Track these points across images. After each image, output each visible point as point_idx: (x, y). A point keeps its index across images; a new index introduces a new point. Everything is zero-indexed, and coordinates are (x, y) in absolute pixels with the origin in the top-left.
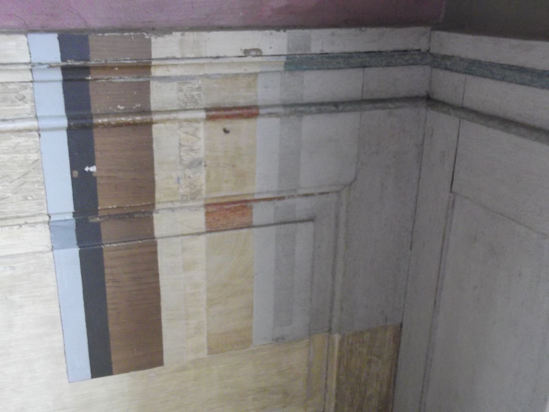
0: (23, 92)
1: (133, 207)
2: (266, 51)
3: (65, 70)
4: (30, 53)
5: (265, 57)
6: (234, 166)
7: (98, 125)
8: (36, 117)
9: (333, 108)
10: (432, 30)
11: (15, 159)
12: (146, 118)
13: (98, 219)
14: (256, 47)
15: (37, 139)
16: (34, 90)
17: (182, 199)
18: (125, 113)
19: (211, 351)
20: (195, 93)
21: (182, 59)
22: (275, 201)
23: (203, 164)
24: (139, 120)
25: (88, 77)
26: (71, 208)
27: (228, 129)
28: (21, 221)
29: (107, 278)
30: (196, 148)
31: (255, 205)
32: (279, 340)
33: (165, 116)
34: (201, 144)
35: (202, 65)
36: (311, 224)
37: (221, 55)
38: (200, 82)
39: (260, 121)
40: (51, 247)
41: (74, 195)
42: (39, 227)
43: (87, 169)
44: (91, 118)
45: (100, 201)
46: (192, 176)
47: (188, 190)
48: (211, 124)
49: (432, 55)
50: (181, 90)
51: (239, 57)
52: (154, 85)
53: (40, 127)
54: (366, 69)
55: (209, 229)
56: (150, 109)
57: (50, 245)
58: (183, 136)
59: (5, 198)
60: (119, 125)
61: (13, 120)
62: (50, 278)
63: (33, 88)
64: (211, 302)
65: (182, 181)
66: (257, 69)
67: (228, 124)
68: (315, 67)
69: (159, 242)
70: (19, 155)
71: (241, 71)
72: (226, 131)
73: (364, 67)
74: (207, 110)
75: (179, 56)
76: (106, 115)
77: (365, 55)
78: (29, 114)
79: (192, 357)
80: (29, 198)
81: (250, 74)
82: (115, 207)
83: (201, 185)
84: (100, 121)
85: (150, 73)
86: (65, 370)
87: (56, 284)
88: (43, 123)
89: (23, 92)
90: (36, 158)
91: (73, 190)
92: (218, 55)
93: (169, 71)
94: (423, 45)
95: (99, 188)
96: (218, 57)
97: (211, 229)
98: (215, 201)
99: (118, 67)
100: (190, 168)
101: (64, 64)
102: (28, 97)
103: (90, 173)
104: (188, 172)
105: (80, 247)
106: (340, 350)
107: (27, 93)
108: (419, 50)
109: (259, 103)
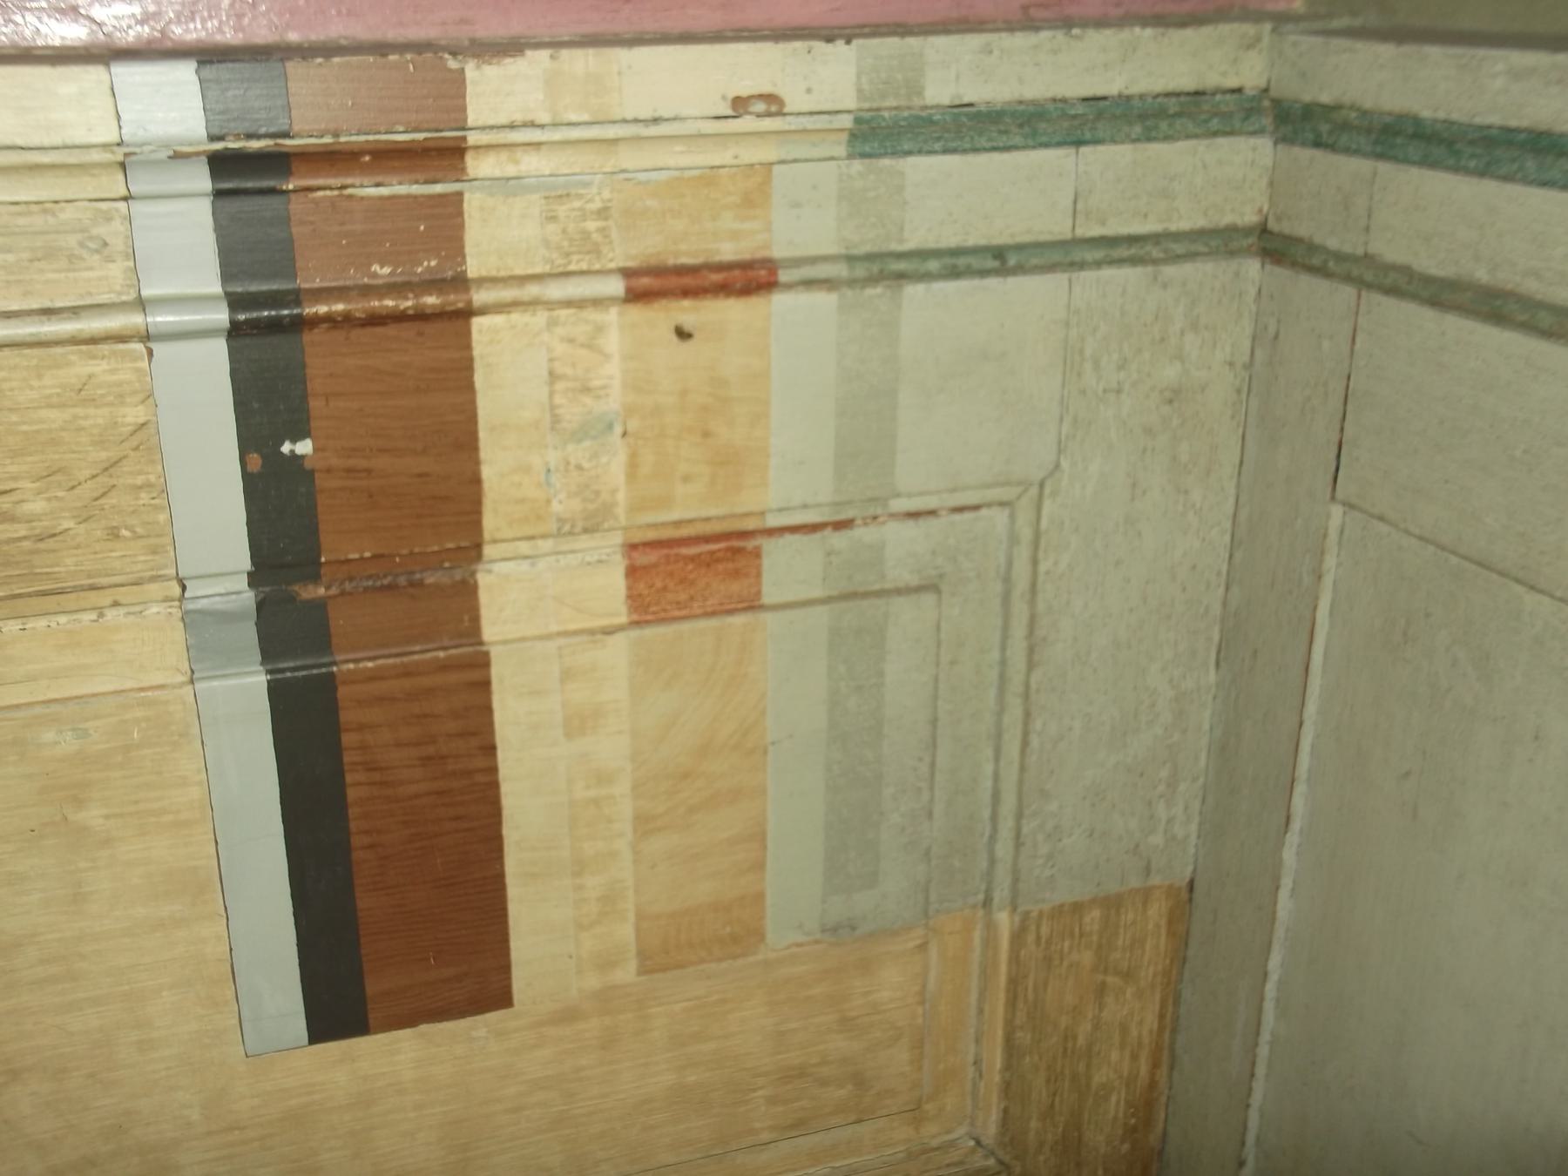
2: (795, 100)
6: (706, 434)
12: (455, 300)
14: (766, 89)
17: (559, 529)
20: (592, 225)
22: (828, 532)
23: (618, 430)
24: (433, 306)
27: (687, 328)
29: (347, 758)
30: (596, 383)
31: (769, 546)
34: (612, 371)
36: (928, 599)
40: (189, 672)
43: (286, 448)
45: (326, 540)
46: (586, 465)
50: (553, 219)
54: (1084, 150)
55: (635, 617)
58: (560, 349)
59: (54, 535)
64: (645, 825)
67: (687, 312)
68: (937, 146)
70: (92, 411)
72: (683, 334)
73: (1079, 143)
74: (627, 273)
75: (544, 117)
78: (120, 293)
79: (593, 982)
80: (125, 533)
82: (367, 554)
85: (463, 170)
89: (101, 230)
90: (141, 420)
92: (657, 115)
93: (517, 162)
96: (656, 121)
102: (118, 244)
104: (578, 452)
105: (269, 672)
109: (777, 253)
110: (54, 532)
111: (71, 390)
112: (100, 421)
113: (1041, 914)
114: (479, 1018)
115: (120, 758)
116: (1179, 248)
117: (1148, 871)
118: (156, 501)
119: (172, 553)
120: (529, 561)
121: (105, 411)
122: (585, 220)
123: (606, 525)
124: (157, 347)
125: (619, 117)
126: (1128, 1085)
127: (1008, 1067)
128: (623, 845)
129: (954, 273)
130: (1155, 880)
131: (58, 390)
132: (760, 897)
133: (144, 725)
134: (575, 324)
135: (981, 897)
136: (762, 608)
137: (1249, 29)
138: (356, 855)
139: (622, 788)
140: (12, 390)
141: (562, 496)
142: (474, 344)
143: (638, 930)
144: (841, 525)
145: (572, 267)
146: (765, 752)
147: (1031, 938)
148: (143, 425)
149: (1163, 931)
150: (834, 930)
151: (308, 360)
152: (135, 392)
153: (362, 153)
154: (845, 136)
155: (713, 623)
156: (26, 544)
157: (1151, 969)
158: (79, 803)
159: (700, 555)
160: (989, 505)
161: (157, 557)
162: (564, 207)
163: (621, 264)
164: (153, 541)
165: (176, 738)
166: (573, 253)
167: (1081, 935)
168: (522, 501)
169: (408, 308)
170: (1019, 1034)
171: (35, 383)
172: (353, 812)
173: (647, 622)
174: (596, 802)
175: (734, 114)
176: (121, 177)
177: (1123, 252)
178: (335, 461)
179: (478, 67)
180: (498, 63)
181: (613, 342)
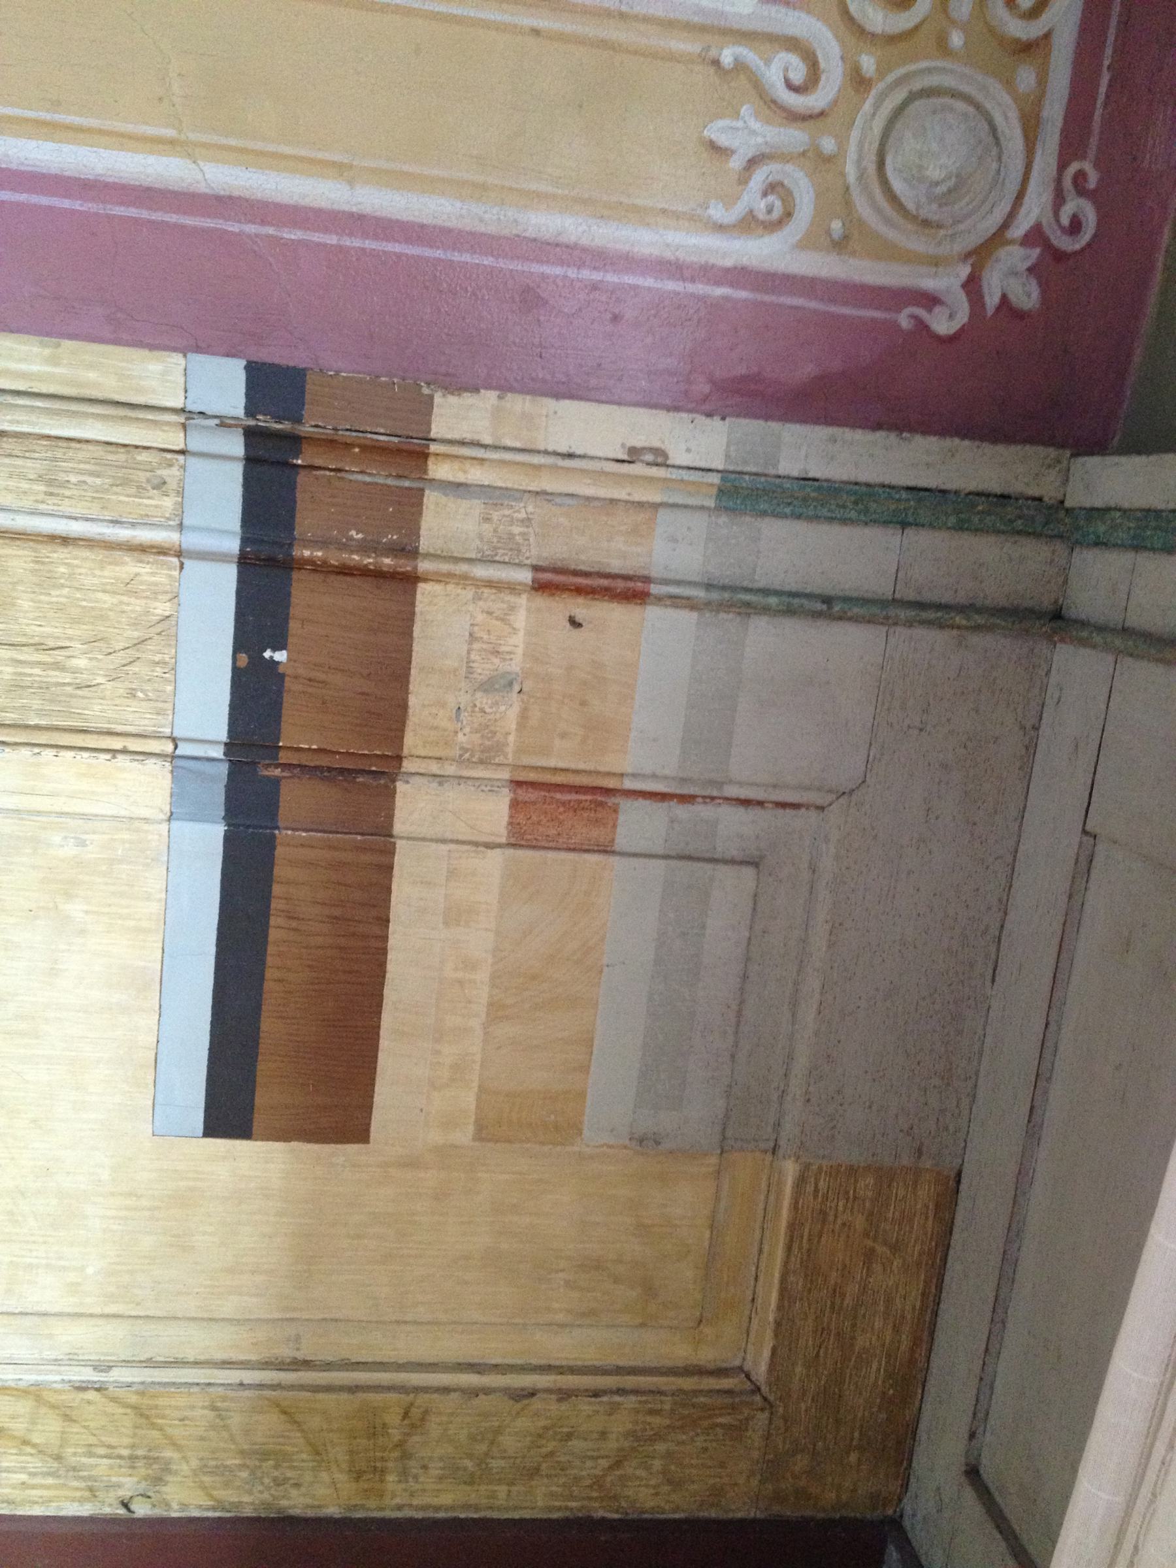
0: (164, 473)
1: (353, 753)
2: (678, 457)
3: (252, 435)
4: (186, 392)
5: (674, 471)
6: (583, 703)
7: (302, 564)
8: (181, 526)
9: (820, 606)
10: (1073, 455)
11: (125, 608)
12: (405, 566)
13: (277, 772)
14: (656, 443)
15: (176, 573)
16: (185, 471)
17: (461, 756)
18: (364, 548)
19: (482, 1133)
20: (516, 530)
21: (496, 448)
22: (674, 803)
23: (517, 688)
24: (389, 566)
25: (297, 459)
26: (219, 730)
27: (579, 619)
28: (117, 744)
29: (275, 904)
30: (503, 649)
31: (625, 804)
32: (645, 1142)
33: (445, 567)
34: (517, 642)
35: (538, 467)
36: (748, 872)
37: (579, 452)
38: (530, 509)
39: (652, 612)
40: (169, 814)
41: (233, 707)
42: (152, 764)
43: (267, 654)
44: (291, 545)
45: (286, 727)
46: (488, 710)
47: (476, 738)
48: (542, 601)
49: (1068, 511)
50: (487, 520)
51: (618, 461)
52: (431, 498)
53: (184, 546)
54: (910, 532)
55: (513, 841)
56: (417, 548)
57: (167, 809)
58: (480, 618)
59: (89, 686)
60: (345, 571)
61: (133, 525)
62: (154, 881)
63: (183, 467)
64: (497, 1012)
65: (464, 715)
66: (657, 498)
67: (581, 608)
68: (788, 510)
69: (400, 845)
70: (132, 600)
71: (621, 494)
72: (575, 623)
73: (904, 525)
74: (536, 568)
75: (487, 439)
76: (323, 544)
77: (904, 495)
78: (168, 519)
79: (436, 1137)
80: (140, 694)
81: (641, 505)
82: (314, 747)
83: (508, 734)
84: (307, 553)
85: (425, 472)
86: (150, 1103)
87: (163, 896)
88: (192, 541)
89: (164, 473)
90: (167, 614)
91: (233, 694)
92: (571, 451)
93: (465, 472)
94: (1048, 488)
95: (287, 699)
96: (571, 456)
97: (519, 838)
98: (532, 776)
99: (359, 446)
100: (485, 691)
101: (252, 423)
102: (173, 484)
103: (273, 663)
104: (483, 700)
105: (228, 825)
106: (795, 1206)
107: (171, 474)
108: (1040, 499)
109: (654, 574)
110: (89, 684)
111: (122, 583)
112: (138, 608)
113: (820, 1168)
114: (339, 1146)
115: (104, 868)
116: (980, 620)
117: (920, 1152)
118: (167, 675)
119: (171, 717)
120: (438, 779)
121: (143, 602)
122: (511, 525)
123: (497, 761)
124: (188, 563)
125: (542, 448)
126: (889, 1356)
127: (780, 1308)
128: (476, 1024)
129: (790, 612)
130: (928, 1164)
131: (113, 581)
132: (582, 1095)
133: (127, 846)
134: (496, 602)
135: (772, 1144)
136: (613, 853)
137: (1052, 452)
138: (268, 985)
139: (482, 976)
140: (80, 574)
141: (467, 730)
142: (417, 603)
143: (478, 1099)
144: (686, 799)
145: (497, 558)
146: (601, 972)
147: (810, 1188)
148: (168, 617)
149: (931, 1214)
150: (641, 1141)
151: (293, 592)
152: (167, 592)
153: (352, 445)
154: (714, 491)
155: (571, 856)
156: (69, 689)
157: (918, 1248)
158: (68, 896)
159: (570, 801)
160: (807, 807)
161: (160, 717)
162: (497, 513)
163: (534, 563)
164: (160, 705)
165: (149, 861)
166: (499, 548)
167: (855, 1198)
168: (436, 728)
169: (370, 563)
170: (792, 1278)
171: (97, 572)
172: (271, 949)
173: (521, 846)
174: (460, 982)
175: (629, 459)
176: (182, 435)
177: (931, 615)
178: (301, 671)
179: (444, 396)
180: (459, 395)
181: (520, 619)
